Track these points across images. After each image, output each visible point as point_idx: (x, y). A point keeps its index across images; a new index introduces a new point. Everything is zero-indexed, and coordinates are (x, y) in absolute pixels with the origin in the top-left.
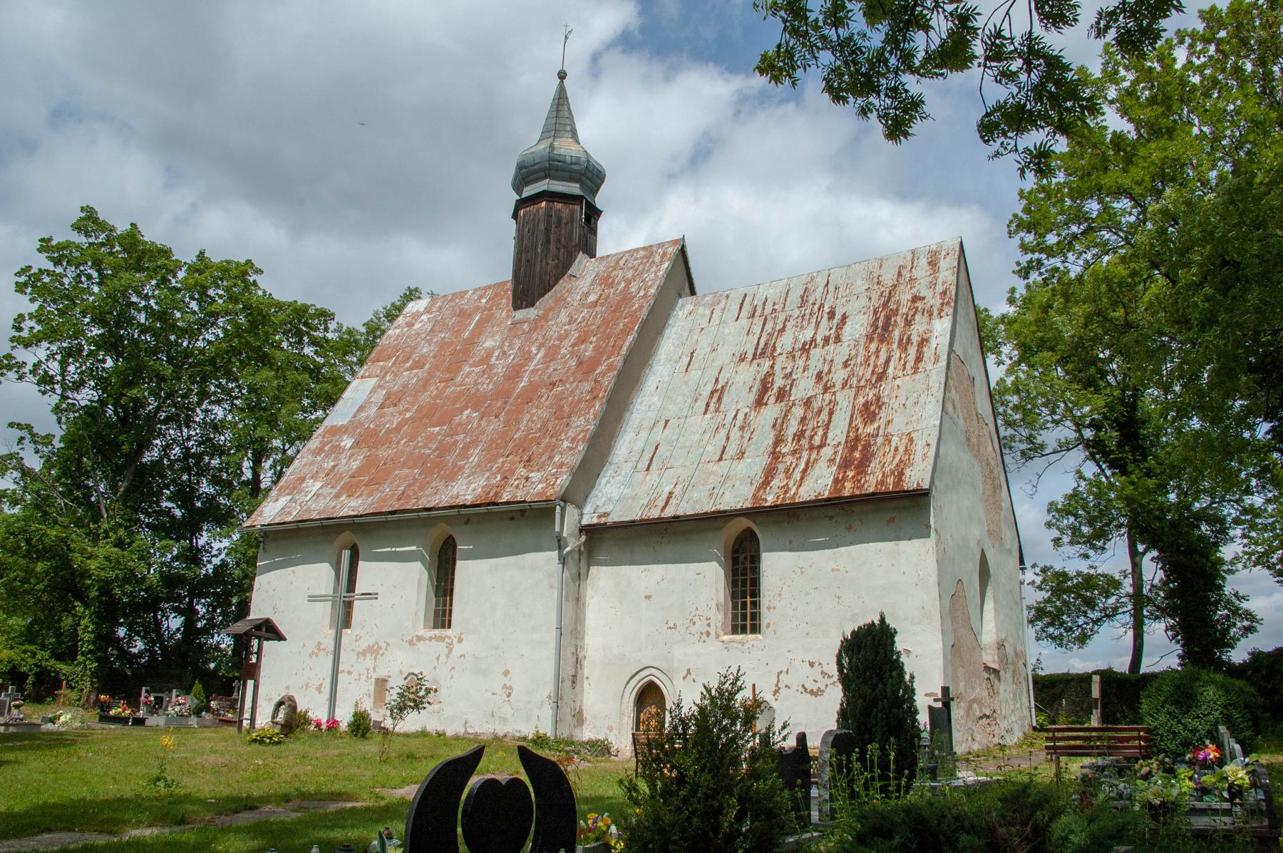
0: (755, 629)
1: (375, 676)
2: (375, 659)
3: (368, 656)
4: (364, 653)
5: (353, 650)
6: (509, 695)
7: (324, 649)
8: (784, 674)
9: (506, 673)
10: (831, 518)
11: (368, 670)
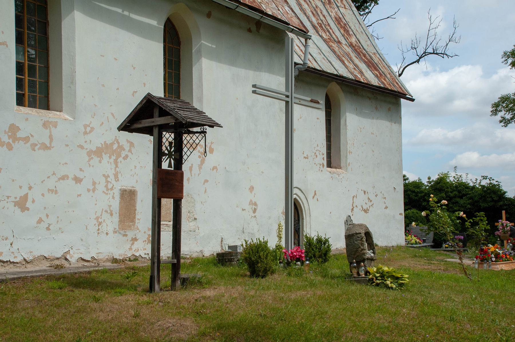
0: (339, 167)
1: (118, 186)
2: (116, 162)
3: (106, 157)
4: (99, 152)
5: (82, 147)
6: (255, 211)
7: (26, 139)
8: (355, 197)
9: (252, 189)
10: (370, 99)
11: (106, 177)
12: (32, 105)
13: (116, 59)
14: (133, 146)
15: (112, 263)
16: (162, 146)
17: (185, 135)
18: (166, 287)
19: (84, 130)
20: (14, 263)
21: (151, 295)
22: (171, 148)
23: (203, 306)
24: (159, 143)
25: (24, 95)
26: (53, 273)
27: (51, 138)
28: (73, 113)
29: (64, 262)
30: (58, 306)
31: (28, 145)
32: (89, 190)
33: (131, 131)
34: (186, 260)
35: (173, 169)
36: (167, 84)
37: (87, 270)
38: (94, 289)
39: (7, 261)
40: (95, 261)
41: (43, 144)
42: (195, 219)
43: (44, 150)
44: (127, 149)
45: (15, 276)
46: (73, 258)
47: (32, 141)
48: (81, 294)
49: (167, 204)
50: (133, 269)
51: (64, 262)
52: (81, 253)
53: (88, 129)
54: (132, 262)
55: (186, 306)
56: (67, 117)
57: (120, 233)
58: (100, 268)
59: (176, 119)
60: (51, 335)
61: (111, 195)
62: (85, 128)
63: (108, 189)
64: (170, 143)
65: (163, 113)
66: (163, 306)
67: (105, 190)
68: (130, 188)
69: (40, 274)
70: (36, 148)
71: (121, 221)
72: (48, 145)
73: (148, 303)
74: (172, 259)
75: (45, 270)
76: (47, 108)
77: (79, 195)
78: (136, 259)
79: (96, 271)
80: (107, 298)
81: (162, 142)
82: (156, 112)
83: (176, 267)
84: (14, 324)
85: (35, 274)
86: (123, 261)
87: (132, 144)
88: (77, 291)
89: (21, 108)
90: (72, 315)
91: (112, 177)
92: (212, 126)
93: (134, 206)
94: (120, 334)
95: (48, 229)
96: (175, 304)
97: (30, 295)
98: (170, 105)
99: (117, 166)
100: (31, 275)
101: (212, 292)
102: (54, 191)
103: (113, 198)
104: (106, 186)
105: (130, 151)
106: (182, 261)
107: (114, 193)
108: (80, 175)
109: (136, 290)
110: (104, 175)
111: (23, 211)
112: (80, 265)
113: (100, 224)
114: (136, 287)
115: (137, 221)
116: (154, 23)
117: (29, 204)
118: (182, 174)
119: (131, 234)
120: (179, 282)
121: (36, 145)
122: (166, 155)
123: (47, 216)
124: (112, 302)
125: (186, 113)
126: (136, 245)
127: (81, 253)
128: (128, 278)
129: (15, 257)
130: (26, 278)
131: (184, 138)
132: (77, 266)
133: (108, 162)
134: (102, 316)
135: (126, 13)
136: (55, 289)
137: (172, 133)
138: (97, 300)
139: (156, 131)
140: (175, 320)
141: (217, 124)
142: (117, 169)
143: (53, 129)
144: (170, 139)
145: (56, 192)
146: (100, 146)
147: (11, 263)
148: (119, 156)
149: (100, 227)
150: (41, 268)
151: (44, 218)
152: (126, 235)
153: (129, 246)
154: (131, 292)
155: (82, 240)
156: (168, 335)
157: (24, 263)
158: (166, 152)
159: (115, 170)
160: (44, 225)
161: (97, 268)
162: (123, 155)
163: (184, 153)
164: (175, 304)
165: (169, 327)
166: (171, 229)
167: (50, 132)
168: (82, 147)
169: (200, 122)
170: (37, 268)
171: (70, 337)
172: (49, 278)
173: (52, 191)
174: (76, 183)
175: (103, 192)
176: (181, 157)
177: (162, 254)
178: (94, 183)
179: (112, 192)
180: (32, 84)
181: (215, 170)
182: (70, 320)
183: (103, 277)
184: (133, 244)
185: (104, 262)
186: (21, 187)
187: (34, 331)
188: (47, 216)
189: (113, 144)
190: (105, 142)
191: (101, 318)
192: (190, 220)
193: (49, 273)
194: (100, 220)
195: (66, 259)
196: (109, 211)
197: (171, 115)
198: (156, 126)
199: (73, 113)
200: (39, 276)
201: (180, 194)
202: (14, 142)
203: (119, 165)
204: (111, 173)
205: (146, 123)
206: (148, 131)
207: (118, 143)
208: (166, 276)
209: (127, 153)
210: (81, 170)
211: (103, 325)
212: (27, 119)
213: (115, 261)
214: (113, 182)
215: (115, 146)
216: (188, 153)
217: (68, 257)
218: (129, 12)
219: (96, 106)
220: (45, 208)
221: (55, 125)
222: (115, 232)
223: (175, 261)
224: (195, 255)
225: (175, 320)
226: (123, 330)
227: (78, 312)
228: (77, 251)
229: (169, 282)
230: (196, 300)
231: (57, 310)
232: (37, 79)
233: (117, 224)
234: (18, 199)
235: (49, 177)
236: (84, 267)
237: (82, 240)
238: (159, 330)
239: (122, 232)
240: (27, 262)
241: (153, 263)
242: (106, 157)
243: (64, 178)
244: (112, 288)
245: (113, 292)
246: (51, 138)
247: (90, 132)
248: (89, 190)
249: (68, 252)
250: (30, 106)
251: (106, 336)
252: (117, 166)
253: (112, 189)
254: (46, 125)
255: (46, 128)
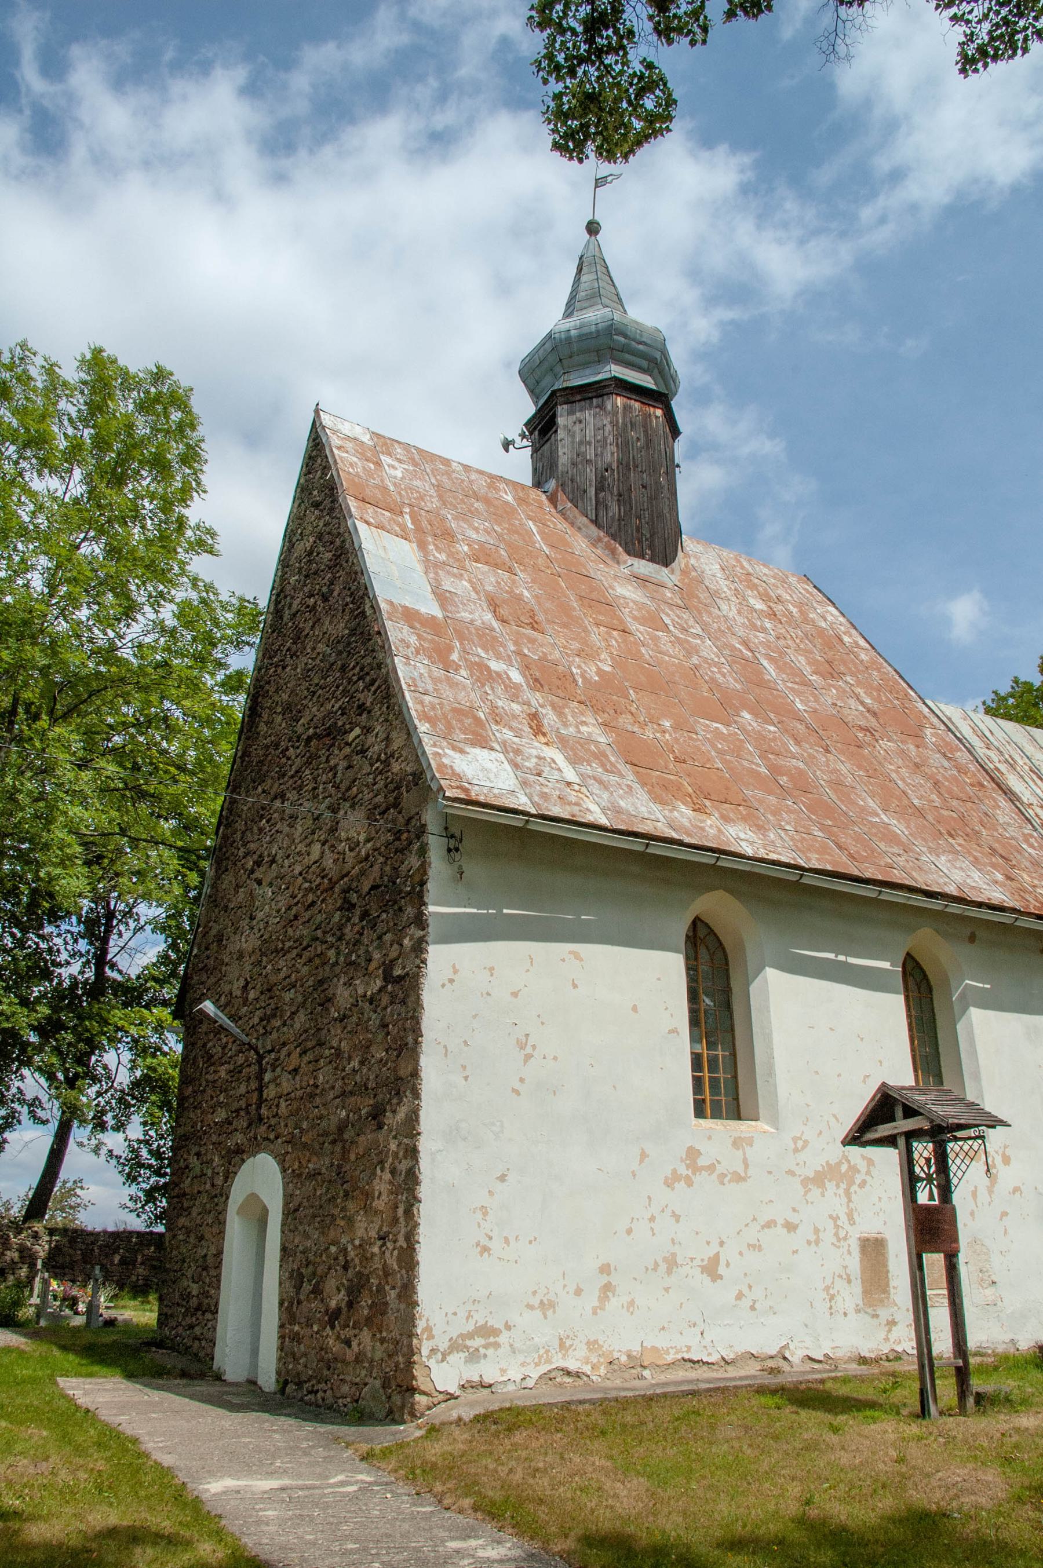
1: (855, 1234)
3: (830, 1186)
4: (819, 1180)
5: (791, 1173)
7: (711, 1168)
11: (835, 1219)
12: (716, 1115)
13: (832, 1029)
14: (873, 1165)
15: (859, 1364)
16: (914, 1165)
17: (951, 1144)
18: (950, 1409)
19: (792, 1146)
20: (708, 1363)
21: (924, 1422)
22: (929, 1168)
23: (1016, 1446)
24: (909, 1162)
25: (704, 1100)
26: (766, 1382)
27: (746, 1163)
28: (774, 1121)
29: (782, 1363)
30: (776, 1438)
31: (714, 1176)
32: (809, 1243)
33: (864, 1144)
34: (985, 1359)
35: (937, 1203)
36: (918, 1058)
37: (818, 1376)
38: (829, 1411)
39: (698, 1362)
40: (830, 1362)
41: (735, 1173)
42: (994, 1283)
43: (737, 1182)
44: (864, 1170)
45: (712, 1386)
46: (796, 1356)
47: (719, 1169)
48: (810, 1419)
49: (934, 1262)
50: (894, 1374)
51: (782, 1363)
52: (807, 1348)
53: (800, 1144)
54: (891, 1364)
55: (985, 1445)
56: (767, 1127)
57: (866, 1313)
58: (839, 1374)
59: (932, 1121)
60: (767, 1485)
61: (845, 1250)
62: (795, 1143)
63: (840, 1238)
64: (928, 1160)
65: (910, 1112)
66: (945, 1444)
67: (834, 1240)
68: (876, 1235)
69: (746, 1382)
70: (726, 1180)
71: (866, 1292)
72: (743, 1174)
73: (920, 1439)
74: (955, 1358)
75: (754, 1377)
76: (739, 1117)
77: (795, 1252)
78: (898, 1358)
79: (834, 1379)
80: (851, 1426)
81: (913, 1159)
82: (899, 1112)
83: (962, 1374)
84: (714, 1464)
85: (739, 1383)
86: (877, 1360)
87: (870, 1162)
88: (804, 1414)
89: (702, 1121)
90: (798, 1455)
91: (844, 1218)
92: (993, 1127)
93: (885, 1265)
94: (875, 1491)
95: (753, 1308)
96: (965, 1441)
97: (734, 1418)
98: (919, 1099)
99: (850, 1200)
100: (734, 1383)
101: (1032, 1419)
102: (756, 1247)
103: (849, 1253)
104: (836, 1234)
105: (868, 1173)
106: (972, 1361)
107: (849, 1246)
108: (794, 1219)
109: (898, 1413)
110: (831, 1217)
111: (714, 1280)
112: (808, 1369)
113: (832, 1297)
114: (897, 1407)
115: (892, 1291)
116: (886, 965)
117: (721, 1270)
118: (954, 1209)
119: (884, 1314)
120: (971, 1401)
121: (726, 1176)
122: (922, 1179)
123: (750, 1287)
124: (859, 1435)
125: (946, 1108)
126: (894, 1334)
127: (807, 1348)
128: (885, 1391)
129: (709, 1354)
130: (723, 1390)
131: (949, 1150)
132: (802, 1369)
133: (835, 1194)
134: (845, 1459)
135: (842, 958)
136: (770, 1408)
137: (928, 1142)
138: (835, 1430)
139: (901, 1141)
140: (966, 1471)
141: (1002, 1121)
142: (851, 1204)
143: (748, 1149)
144: (926, 1154)
145: (760, 1249)
146: (820, 1169)
147: (704, 1363)
148: (851, 1183)
149: (833, 1303)
150: (748, 1373)
151: (746, 1291)
152: (877, 1316)
153: (883, 1335)
154: (891, 1417)
155: (806, 1326)
156: (956, 1497)
157: (723, 1363)
158: (923, 1175)
159: (848, 1206)
160: (746, 1303)
161: (833, 1374)
162: (858, 1181)
163: (952, 1175)
164: (965, 1441)
165: (957, 1482)
166: (946, 1302)
167: (744, 1154)
168: (791, 1173)
169: (971, 1122)
170: (742, 1373)
171: (796, 1490)
172: (761, 1390)
173: (753, 1246)
174: (789, 1231)
175: (833, 1244)
176: (948, 1181)
177: (935, 1351)
178: (816, 1231)
179: (845, 1244)
180: (714, 1083)
181: (1018, 1194)
182: (795, 1462)
183: (844, 1390)
184: (890, 1331)
185: (845, 1363)
186: (708, 1243)
187: (743, 1477)
188: (750, 1287)
189: (839, 1164)
190: (827, 1162)
191: (844, 1461)
192: (985, 1286)
193: (759, 1381)
194: (831, 1291)
195: (785, 1358)
196: (844, 1276)
197: (921, 1114)
198: (900, 1134)
199: (774, 1121)
200: (746, 1386)
201: (954, 1245)
202: (694, 1174)
203: (854, 1197)
204: (842, 1212)
205: (884, 1130)
206: (890, 1141)
207: (849, 1162)
208: (946, 1389)
209: (864, 1177)
210: (794, 1210)
211: (846, 1473)
212: (710, 1138)
213: (863, 1360)
214: (847, 1227)
215: (844, 1168)
216: (959, 1174)
217: (787, 1355)
218: (846, 955)
219: (808, 1105)
220: (746, 1274)
221: (750, 1142)
222: (858, 1311)
223: (960, 1362)
224: (1000, 1349)
225: (966, 1471)
226: (879, 1485)
227: (807, 1448)
228: (800, 1345)
229: (954, 1401)
230: (1003, 1434)
231: (774, 1445)
232: (721, 1075)
233: (861, 1296)
234: (706, 1262)
235: (747, 1225)
236: (814, 1371)
237: (806, 1326)
238: (940, 1487)
239: (870, 1310)
240: (727, 1363)
241: (922, 1366)
242: (830, 1186)
243: (770, 1224)
244: (859, 1410)
245: (861, 1415)
246: (746, 1163)
247: (804, 1147)
248: (809, 1243)
249: (786, 1347)
250: (713, 1117)
251: (853, 1493)
252: (850, 1200)
253: (845, 1239)
254: (737, 1143)
255: (738, 1149)
